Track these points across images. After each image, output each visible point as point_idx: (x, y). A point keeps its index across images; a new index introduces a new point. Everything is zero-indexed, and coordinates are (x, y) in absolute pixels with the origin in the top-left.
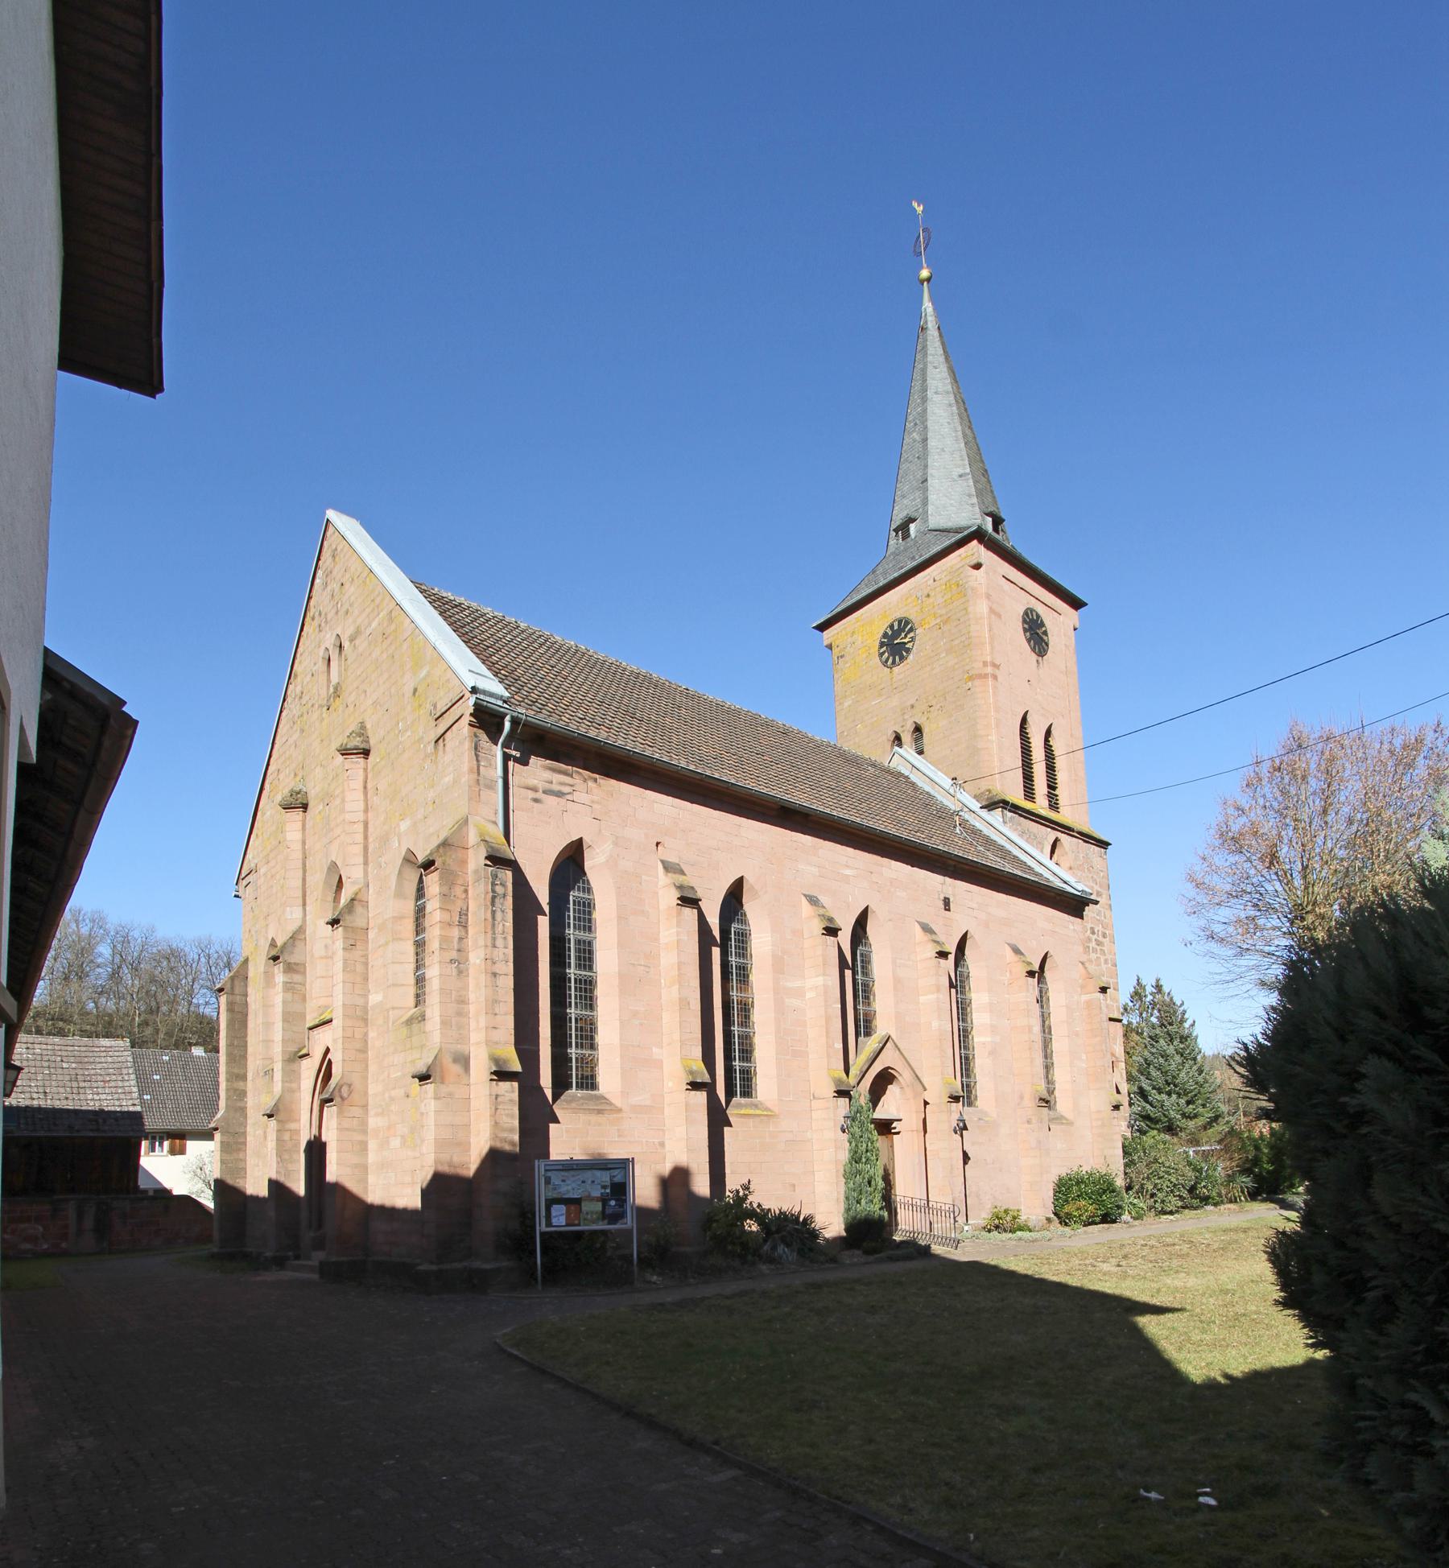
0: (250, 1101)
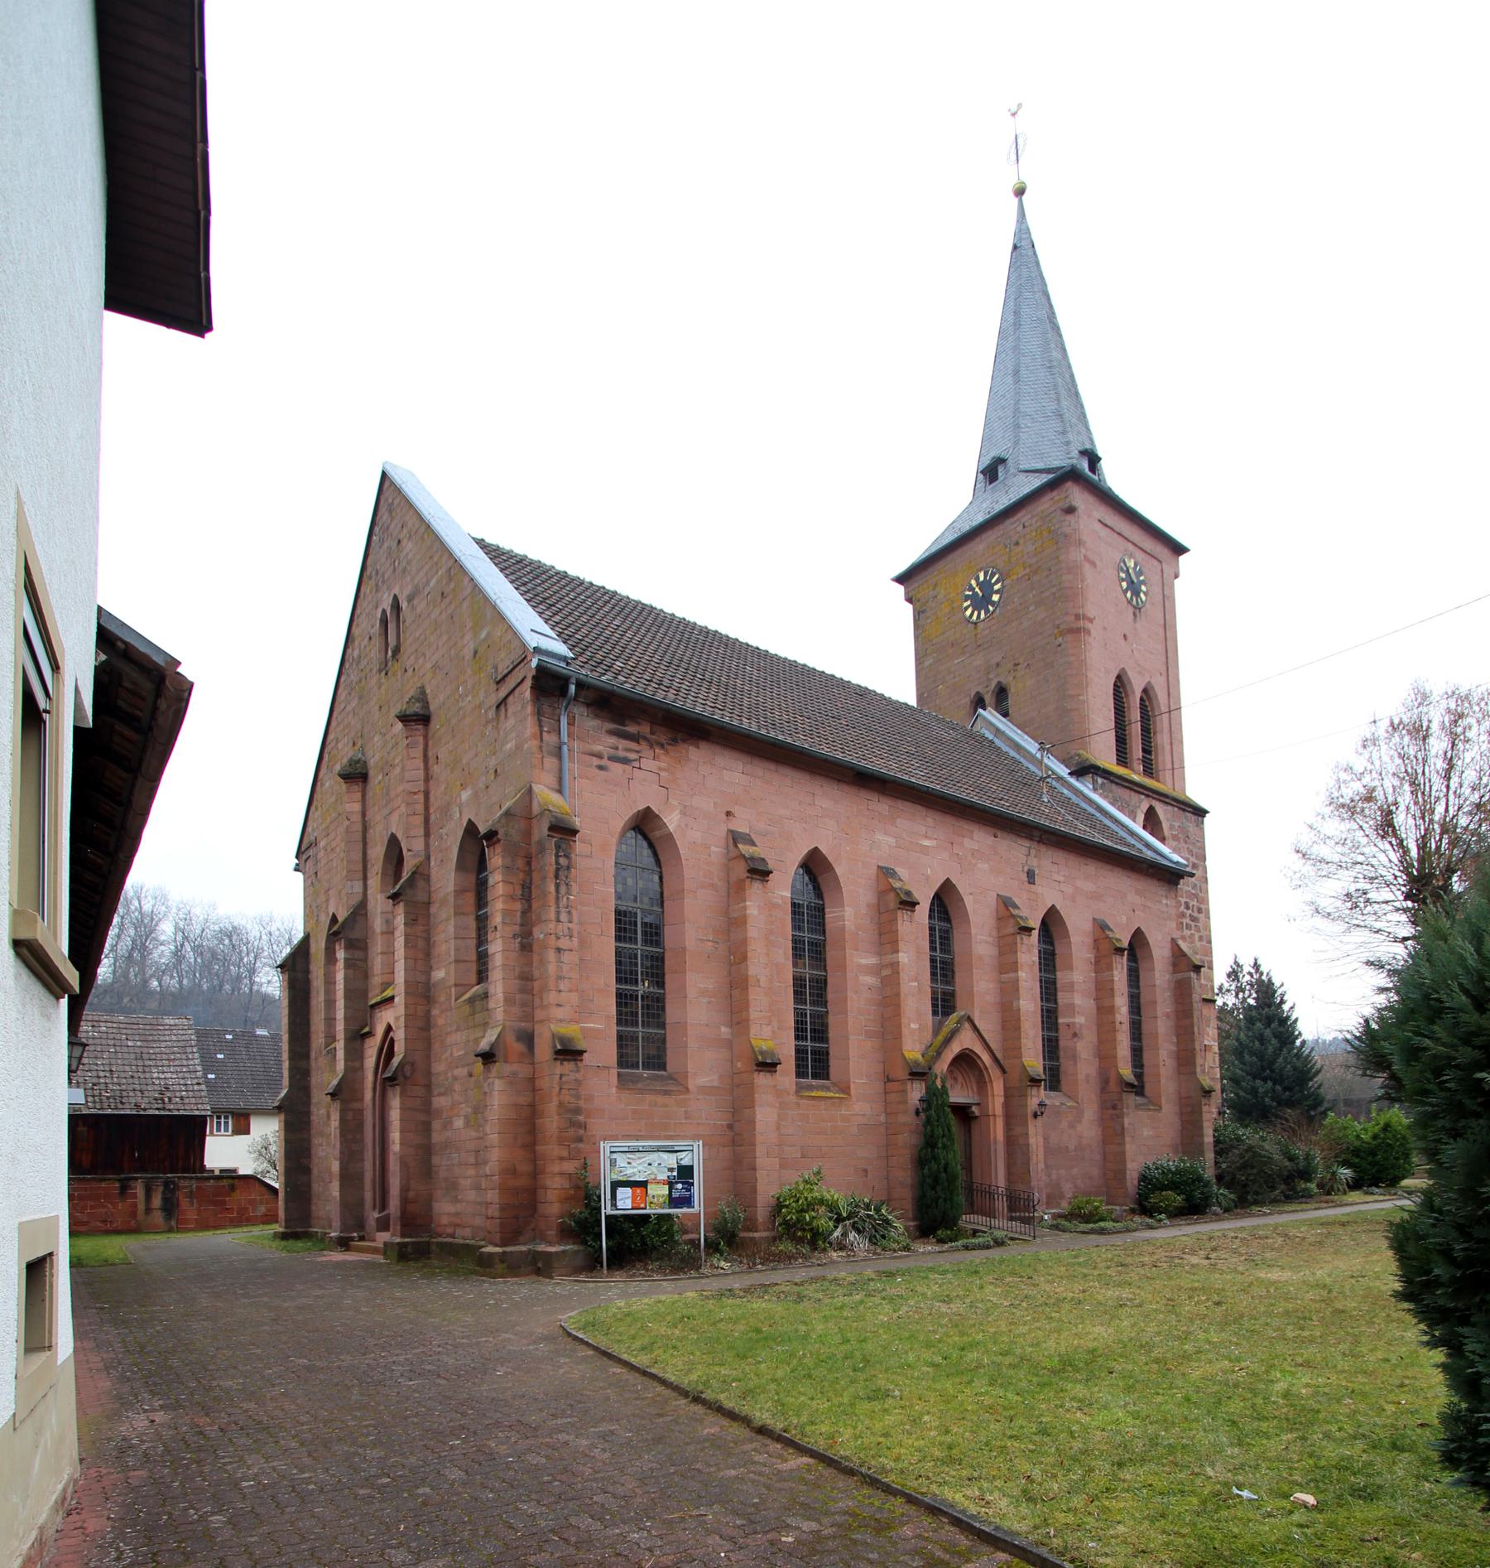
0: (315, 1079)
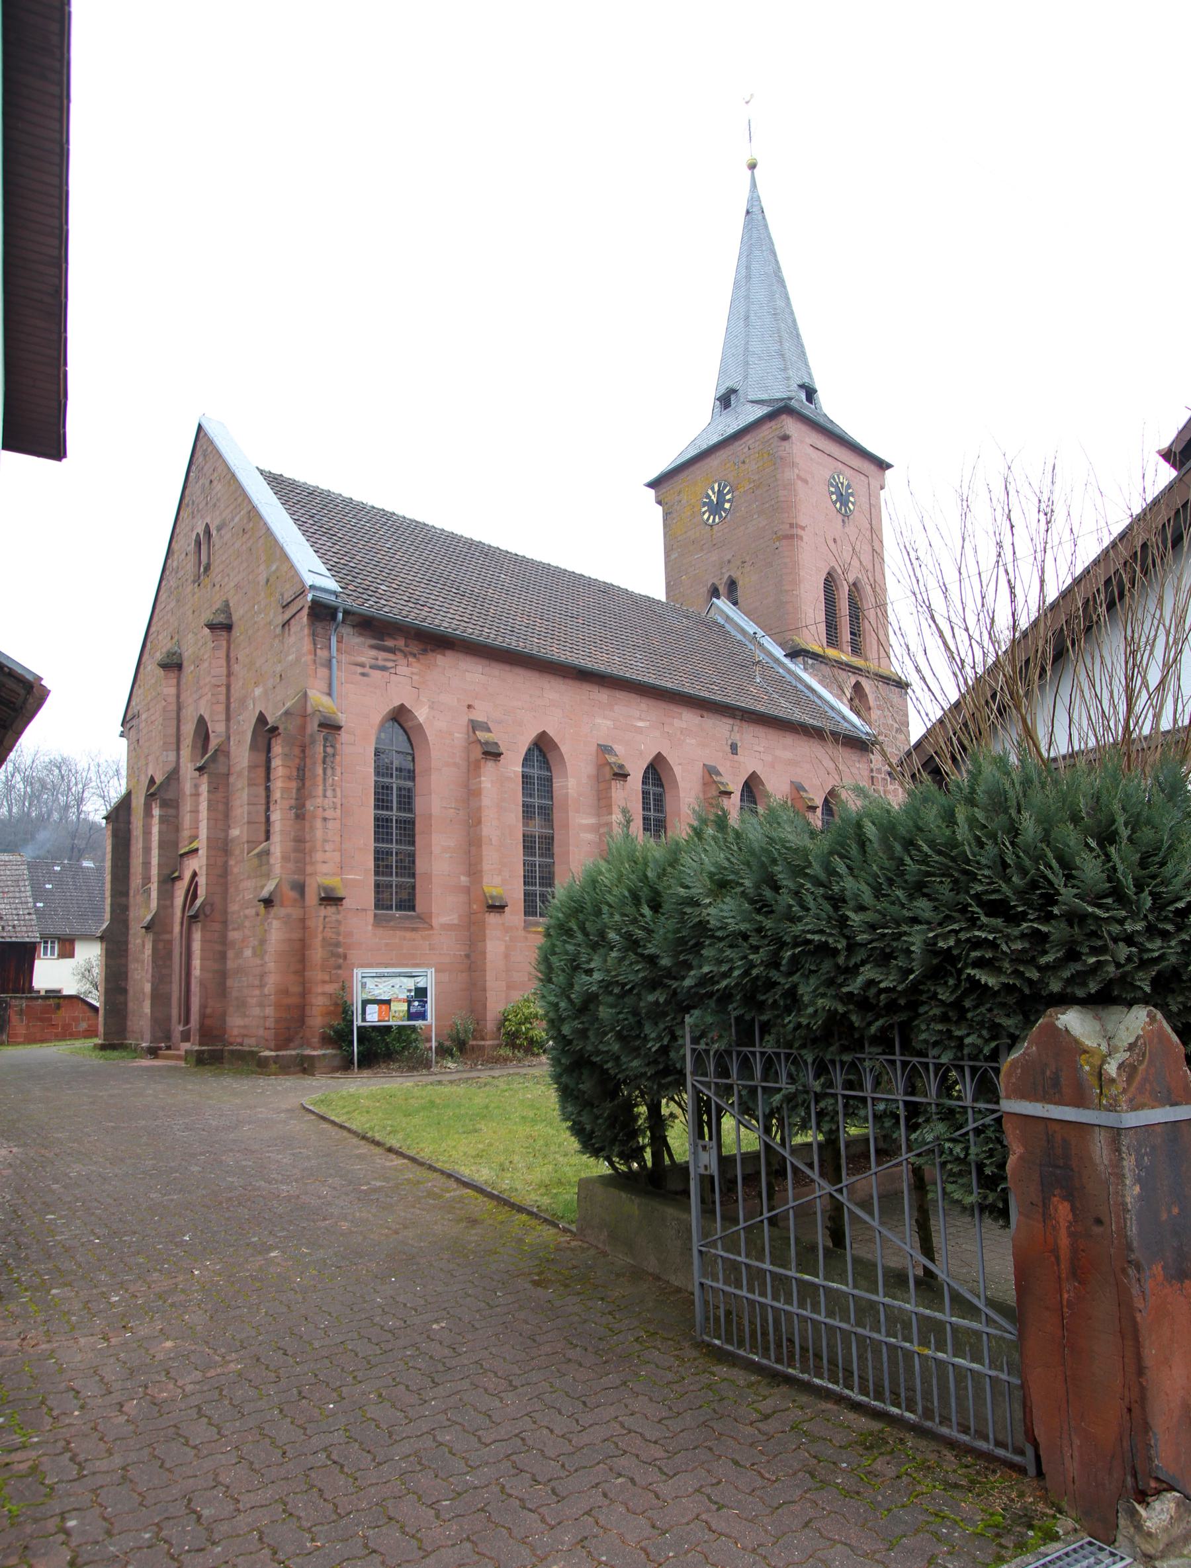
0: (133, 914)
